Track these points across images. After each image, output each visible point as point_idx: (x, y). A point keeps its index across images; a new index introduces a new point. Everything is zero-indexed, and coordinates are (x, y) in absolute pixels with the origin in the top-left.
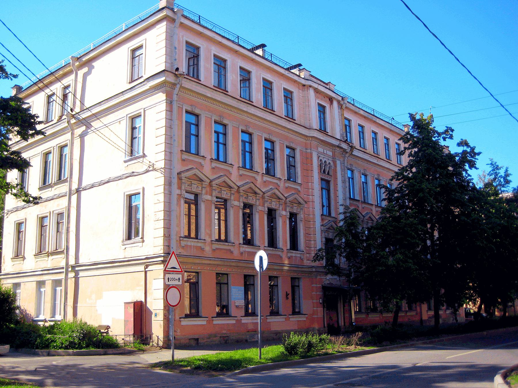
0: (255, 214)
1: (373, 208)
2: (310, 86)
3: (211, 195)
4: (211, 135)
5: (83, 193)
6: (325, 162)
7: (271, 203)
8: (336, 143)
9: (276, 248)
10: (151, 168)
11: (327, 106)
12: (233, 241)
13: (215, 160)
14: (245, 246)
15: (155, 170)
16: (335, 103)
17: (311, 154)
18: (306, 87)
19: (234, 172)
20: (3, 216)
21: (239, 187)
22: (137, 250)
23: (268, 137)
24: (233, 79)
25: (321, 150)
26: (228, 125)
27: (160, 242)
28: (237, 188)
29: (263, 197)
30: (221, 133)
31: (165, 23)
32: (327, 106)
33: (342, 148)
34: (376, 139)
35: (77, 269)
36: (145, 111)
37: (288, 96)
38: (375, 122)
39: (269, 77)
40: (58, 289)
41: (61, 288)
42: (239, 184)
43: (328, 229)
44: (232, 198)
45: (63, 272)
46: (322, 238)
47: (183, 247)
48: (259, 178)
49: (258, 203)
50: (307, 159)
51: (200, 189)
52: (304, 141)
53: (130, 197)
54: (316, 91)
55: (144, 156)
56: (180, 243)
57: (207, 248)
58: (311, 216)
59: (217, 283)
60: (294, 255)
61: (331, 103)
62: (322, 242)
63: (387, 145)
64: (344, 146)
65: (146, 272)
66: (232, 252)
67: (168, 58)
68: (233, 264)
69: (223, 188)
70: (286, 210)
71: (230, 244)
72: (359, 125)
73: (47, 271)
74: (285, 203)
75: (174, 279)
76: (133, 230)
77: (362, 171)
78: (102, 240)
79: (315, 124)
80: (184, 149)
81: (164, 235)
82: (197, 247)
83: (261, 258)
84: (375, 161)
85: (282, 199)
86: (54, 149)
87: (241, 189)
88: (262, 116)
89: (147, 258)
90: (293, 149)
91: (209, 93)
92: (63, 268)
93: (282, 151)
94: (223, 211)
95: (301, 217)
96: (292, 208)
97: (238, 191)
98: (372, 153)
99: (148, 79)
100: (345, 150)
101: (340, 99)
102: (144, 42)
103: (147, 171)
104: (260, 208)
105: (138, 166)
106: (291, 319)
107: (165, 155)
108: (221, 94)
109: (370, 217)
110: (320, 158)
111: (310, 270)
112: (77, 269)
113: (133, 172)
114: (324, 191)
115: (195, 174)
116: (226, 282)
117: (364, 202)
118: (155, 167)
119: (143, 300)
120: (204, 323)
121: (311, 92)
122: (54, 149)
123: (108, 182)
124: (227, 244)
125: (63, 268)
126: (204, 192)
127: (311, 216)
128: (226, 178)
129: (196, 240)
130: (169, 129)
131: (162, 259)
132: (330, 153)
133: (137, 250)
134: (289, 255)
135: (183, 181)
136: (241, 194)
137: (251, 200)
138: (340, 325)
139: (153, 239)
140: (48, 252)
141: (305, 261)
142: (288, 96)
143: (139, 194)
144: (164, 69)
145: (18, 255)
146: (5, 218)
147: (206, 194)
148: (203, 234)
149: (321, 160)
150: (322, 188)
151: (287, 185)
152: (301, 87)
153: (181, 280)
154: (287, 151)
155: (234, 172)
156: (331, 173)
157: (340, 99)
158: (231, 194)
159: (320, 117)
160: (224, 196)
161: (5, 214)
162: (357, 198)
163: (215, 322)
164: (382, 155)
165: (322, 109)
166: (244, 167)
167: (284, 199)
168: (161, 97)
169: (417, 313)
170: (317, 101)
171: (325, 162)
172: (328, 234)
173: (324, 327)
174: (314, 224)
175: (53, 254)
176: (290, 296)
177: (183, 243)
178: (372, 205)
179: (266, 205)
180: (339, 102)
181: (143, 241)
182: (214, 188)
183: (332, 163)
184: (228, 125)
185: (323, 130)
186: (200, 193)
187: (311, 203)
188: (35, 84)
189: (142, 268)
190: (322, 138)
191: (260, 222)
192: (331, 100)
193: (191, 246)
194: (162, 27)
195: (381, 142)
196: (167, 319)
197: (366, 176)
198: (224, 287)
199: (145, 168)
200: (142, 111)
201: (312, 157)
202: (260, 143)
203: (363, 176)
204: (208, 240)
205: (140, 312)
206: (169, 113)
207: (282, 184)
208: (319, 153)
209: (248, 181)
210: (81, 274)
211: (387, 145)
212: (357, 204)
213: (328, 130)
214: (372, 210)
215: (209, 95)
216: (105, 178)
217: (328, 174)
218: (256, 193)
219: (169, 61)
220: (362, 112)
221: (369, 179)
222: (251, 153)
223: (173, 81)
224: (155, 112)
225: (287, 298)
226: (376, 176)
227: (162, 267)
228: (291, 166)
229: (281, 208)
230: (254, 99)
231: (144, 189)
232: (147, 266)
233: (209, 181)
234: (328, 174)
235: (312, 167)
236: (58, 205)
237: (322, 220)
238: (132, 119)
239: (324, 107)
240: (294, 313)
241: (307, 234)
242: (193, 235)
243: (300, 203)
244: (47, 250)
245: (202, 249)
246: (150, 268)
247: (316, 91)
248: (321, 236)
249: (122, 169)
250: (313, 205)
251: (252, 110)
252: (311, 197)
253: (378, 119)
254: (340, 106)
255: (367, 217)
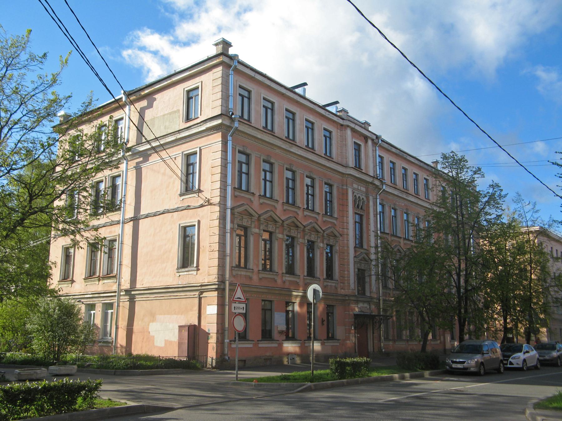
0: (296, 247)
1: (402, 241)
2: (348, 126)
3: (259, 228)
4: (260, 173)
5: (143, 224)
6: (359, 197)
7: (310, 236)
8: (370, 180)
9: (314, 277)
10: (209, 203)
11: (362, 144)
12: (251, 267)
13: (263, 196)
14: (287, 275)
15: (211, 204)
16: (370, 142)
17: (347, 190)
18: (343, 127)
19: (279, 207)
20: (50, 241)
21: (283, 221)
22: (191, 277)
23: (309, 175)
24: (280, 120)
25: (355, 186)
26: (274, 163)
27: (215, 271)
28: (281, 222)
29: (304, 231)
30: (268, 171)
31: (220, 68)
32: (362, 144)
33: (374, 184)
34: (406, 175)
35: (133, 293)
36: (200, 150)
37: (328, 137)
38: (406, 159)
39: (311, 118)
40: (110, 311)
41: (112, 311)
42: (283, 218)
43: (361, 260)
44: (277, 231)
45: (115, 296)
46: (354, 269)
47: (234, 276)
48: (300, 212)
49: (299, 236)
50: (344, 195)
51: (250, 223)
52: (341, 178)
53: (185, 228)
54: (353, 130)
55: (200, 191)
56: (232, 273)
57: (255, 277)
58: (346, 248)
59: (262, 309)
60: (329, 284)
61: (366, 142)
62: (354, 272)
63: (416, 180)
64: (377, 183)
65: (200, 299)
66: (276, 281)
67: (223, 101)
68: (277, 292)
69: (270, 223)
70: (323, 243)
71: (274, 274)
72: (391, 162)
73: (98, 295)
74: (323, 236)
75: (239, 308)
76: (187, 259)
77: (392, 206)
78: (153, 268)
79: (351, 162)
80: (237, 187)
81: (219, 265)
82: (246, 277)
83: (315, 291)
84: (404, 196)
85: (320, 232)
86: (106, 179)
87: (286, 223)
88: (305, 156)
89: (201, 286)
90: (331, 186)
91: (259, 135)
92: (115, 292)
93: (321, 188)
94: (243, 238)
95: (337, 248)
96: (329, 240)
97: (282, 225)
98: (402, 189)
99: (205, 121)
100: (377, 186)
101: (374, 137)
102: (200, 84)
103: (202, 206)
104: (301, 240)
105: (193, 200)
106: (326, 344)
107: (221, 192)
108: (270, 136)
109: (398, 249)
110: (355, 194)
111: (344, 298)
112: (133, 293)
113: (189, 206)
114: (357, 224)
115: (246, 210)
116: (269, 308)
117: (393, 235)
118: (211, 202)
119: (197, 324)
120: (251, 346)
121: (349, 132)
122: (106, 179)
123: (163, 213)
124: (271, 273)
125: (115, 292)
126: (253, 226)
127: (346, 248)
128: (272, 213)
129: (245, 270)
130: (224, 168)
131: (216, 286)
132: (363, 189)
133: (191, 277)
134: (325, 284)
135: (236, 216)
136: (285, 228)
137: (293, 233)
138: (369, 351)
139: (208, 269)
140: (99, 276)
141: (339, 290)
142: (328, 137)
143: (194, 225)
144: (220, 113)
145: (66, 277)
146: (51, 242)
147: (255, 227)
148: (251, 265)
149: (355, 196)
150: (356, 222)
151: (325, 219)
152: (339, 126)
153: (245, 309)
154: (326, 189)
155: (279, 207)
156: (364, 208)
157: (374, 137)
158: (276, 228)
159: (355, 155)
160: (293, 235)
161: (52, 239)
162: (387, 231)
163: (260, 345)
164: (411, 190)
165: (358, 148)
166: (288, 202)
167: (322, 232)
168: (217, 137)
169: (440, 343)
170: (354, 140)
171: (359, 197)
172: (360, 265)
173: (356, 352)
174: (348, 256)
175: (104, 278)
176: (325, 323)
177: (234, 273)
178: (400, 238)
179: (306, 238)
180: (373, 140)
181: (198, 270)
182: (262, 222)
183: (365, 199)
184: (274, 163)
185: (358, 167)
186: (249, 227)
187: (345, 236)
188: (34, 95)
189: (197, 293)
190: (357, 176)
191: (301, 254)
192: (366, 138)
193: (241, 275)
194: (218, 72)
195: (411, 178)
196: (220, 342)
197: (395, 210)
198: (268, 313)
199: (201, 202)
200: (198, 150)
201: (347, 193)
202: (302, 180)
203: (393, 211)
204: (256, 270)
205: (194, 335)
206: (224, 153)
207: (320, 218)
208: (354, 189)
209: (311, 221)
210: (138, 298)
211: (416, 180)
212: (387, 236)
213: (363, 167)
214: (400, 243)
215: (259, 137)
216: (161, 209)
217: (361, 208)
218: (297, 227)
219: (225, 105)
220: (394, 150)
221: (398, 212)
222: (293, 189)
223: (228, 124)
224: (211, 153)
225: (323, 324)
226: (405, 211)
227: (215, 294)
228: (329, 202)
229: (319, 241)
230: (297, 139)
231: (199, 222)
232: (202, 293)
233: (257, 216)
234: (361, 208)
235: (347, 202)
236: (111, 232)
237: (355, 251)
238: (188, 156)
239: (359, 146)
240: (328, 338)
241: (342, 265)
242: (242, 264)
243: (335, 236)
244: (98, 275)
245: (250, 278)
246: (205, 294)
247: (353, 130)
248: (354, 266)
249: (175, 202)
250: (347, 238)
251: (294, 150)
252: (345, 230)
253: (408, 156)
254: (375, 144)
255: (396, 250)
